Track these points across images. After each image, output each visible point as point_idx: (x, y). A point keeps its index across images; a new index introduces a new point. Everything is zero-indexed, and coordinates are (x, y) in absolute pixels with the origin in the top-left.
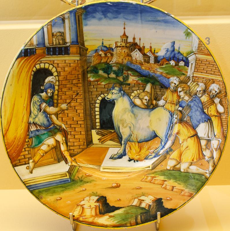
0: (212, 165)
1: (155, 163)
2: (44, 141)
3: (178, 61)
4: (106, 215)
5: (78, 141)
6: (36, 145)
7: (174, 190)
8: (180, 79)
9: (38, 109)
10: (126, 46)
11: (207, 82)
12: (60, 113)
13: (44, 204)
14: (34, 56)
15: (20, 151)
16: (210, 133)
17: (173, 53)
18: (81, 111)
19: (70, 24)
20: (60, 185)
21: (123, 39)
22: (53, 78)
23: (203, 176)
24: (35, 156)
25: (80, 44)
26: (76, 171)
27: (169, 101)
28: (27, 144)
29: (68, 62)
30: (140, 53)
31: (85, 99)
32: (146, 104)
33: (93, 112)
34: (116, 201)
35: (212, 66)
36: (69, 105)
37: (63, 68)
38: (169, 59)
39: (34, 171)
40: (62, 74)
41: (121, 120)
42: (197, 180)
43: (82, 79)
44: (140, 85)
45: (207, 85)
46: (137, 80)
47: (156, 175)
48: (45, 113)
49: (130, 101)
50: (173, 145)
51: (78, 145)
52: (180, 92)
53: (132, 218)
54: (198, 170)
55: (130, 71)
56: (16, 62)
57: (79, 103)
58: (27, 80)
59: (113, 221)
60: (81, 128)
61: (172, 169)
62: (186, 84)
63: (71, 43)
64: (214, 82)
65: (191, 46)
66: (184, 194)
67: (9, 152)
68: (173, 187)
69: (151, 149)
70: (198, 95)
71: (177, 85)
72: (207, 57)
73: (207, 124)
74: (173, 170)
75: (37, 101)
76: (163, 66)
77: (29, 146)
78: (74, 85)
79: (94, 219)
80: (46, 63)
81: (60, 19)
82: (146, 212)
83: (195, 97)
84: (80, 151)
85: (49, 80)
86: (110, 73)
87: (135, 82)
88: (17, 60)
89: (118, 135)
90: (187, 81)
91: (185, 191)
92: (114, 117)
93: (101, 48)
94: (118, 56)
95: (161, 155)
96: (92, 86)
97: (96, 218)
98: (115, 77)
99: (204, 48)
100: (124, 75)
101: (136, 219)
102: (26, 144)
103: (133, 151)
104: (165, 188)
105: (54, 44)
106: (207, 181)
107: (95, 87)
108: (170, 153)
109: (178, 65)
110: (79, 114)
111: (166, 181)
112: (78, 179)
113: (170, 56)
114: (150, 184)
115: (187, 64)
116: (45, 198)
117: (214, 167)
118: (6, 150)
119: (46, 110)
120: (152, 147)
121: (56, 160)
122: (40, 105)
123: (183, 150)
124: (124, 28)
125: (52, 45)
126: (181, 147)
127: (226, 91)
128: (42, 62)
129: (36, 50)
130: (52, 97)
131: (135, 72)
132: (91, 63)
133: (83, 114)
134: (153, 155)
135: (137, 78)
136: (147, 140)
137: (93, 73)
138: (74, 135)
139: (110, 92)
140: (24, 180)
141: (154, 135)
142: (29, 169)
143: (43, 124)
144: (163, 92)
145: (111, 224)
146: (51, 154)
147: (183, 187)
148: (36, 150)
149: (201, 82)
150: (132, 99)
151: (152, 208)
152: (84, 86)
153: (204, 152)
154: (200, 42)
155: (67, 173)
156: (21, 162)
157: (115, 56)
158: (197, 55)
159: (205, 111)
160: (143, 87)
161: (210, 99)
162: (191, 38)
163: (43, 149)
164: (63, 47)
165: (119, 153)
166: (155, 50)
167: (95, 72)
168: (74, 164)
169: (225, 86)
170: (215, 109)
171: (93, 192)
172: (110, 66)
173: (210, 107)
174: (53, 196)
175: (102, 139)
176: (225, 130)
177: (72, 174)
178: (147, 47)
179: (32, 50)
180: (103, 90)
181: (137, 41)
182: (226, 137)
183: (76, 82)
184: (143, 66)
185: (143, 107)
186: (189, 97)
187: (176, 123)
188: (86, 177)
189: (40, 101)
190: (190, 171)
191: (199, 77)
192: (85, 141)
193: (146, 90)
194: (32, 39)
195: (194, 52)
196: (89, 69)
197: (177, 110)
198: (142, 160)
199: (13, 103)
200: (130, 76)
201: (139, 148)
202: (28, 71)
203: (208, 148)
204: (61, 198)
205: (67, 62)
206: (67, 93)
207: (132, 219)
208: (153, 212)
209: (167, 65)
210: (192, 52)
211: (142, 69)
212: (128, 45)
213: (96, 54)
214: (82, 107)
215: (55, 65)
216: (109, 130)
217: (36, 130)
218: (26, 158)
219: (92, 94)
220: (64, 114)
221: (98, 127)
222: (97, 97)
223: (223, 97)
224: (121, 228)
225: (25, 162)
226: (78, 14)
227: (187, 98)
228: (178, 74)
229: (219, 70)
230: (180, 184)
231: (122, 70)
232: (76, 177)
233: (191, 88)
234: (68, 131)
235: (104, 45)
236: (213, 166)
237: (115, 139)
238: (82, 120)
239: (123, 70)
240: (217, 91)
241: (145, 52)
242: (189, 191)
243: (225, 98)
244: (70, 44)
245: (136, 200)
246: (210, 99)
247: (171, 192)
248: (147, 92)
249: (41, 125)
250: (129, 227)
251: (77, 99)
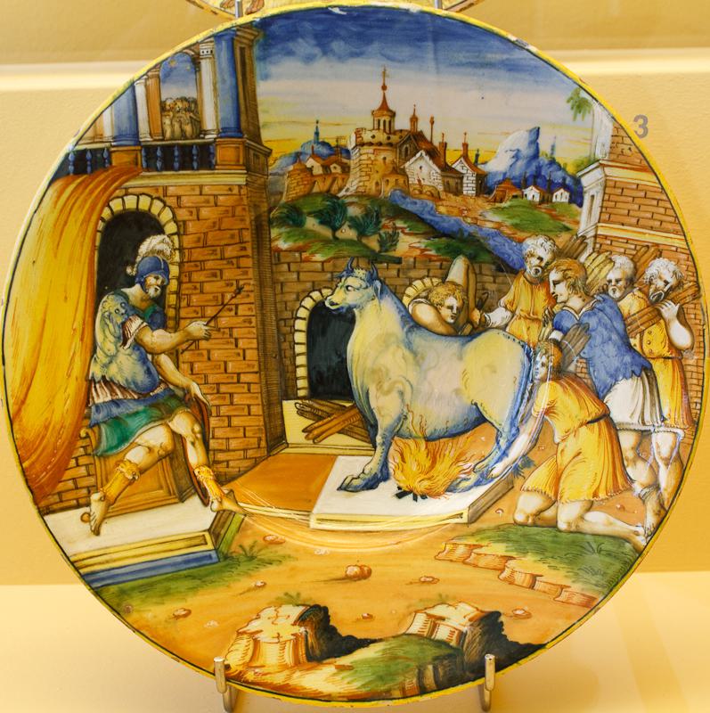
0: (655, 508)
1: (478, 504)
2: (137, 435)
3: (549, 188)
4: (327, 664)
5: (241, 434)
6: (111, 448)
7: (538, 585)
8: (557, 243)
9: (119, 338)
10: (390, 141)
11: (639, 254)
12: (186, 349)
13: (136, 630)
14: (106, 174)
15: (62, 467)
16: (649, 411)
17: (534, 164)
18: (249, 343)
19: (218, 75)
20: (185, 572)
21: (379, 121)
22: (163, 241)
23: (627, 544)
24: (107, 481)
25: (246, 136)
26: (234, 527)
27: (522, 310)
28: (84, 445)
29: (210, 192)
30: (431, 162)
31: (262, 306)
32: (452, 321)
33: (288, 347)
34: (358, 620)
35: (655, 203)
36: (212, 324)
37: (194, 211)
38: (522, 184)
39: (104, 529)
40: (191, 227)
41: (374, 372)
42: (609, 554)
43: (252, 244)
44: (432, 263)
45: (638, 264)
46: (423, 246)
47: (482, 539)
48: (139, 349)
49: (400, 311)
51: (242, 448)
52: (556, 283)
53: (407, 672)
54: (611, 524)
55: (402, 219)
56: (50, 192)
57: (243, 318)
58: (82, 246)
59: (349, 683)
60: (249, 395)
61: (530, 521)
62: (576, 259)
63: (219, 133)
64: (661, 253)
65: (591, 142)
66: (569, 598)
67: (27, 468)
68: (534, 577)
69: (466, 461)
70: (611, 293)
71: (547, 264)
72: (639, 177)
73: (640, 382)
74: (534, 525)
75: (113, 311)
76: (504, 205)
77: (89, 451)
78: (228, 263)
79: (289, 677)
80: (141, 195)
81: (186, 57)
82: (450, 656)
83: (601, 299)
84: (246, 465)
85: (151, 246)
86: (341, 226)
87: (417, 253)
88: (53, 185)
89: (364, 416)
90: (577, 250)
92: (352, 360)
93: (313, 147)
95: (496, 480)
96: (286, 266)
97: (298, 674)
98: (356, 239)
99: (630, 149)
100: (382, 232)
101: (421, 676)
102: (80, 443)
103: (412, 467)
104: (510, 581)
105: (168, 134)
106: (640, 559)
107: (293, 267)
108: (526, 471)
109: (549, 201)
110: (244, 350)
111: (511, 558)
112: (242, 552)
113: (526, 173)
114: (464, 566)
115: (577, 196)
116: (139, 611)
117: (661, 516)
118: (18, 464)
119: (141, 340)
120: (468, 455)
121: (174, 494)
122: (123, 324)
123: (565, 463)
124: (384, 88)
125: (161, 138)
126: (559, 454)
127: (697, 282)
128: (130, 190)
129: (110, 153)
130: (160, 300)
131: (417, 221)
132: (281, 193)
133: (256, 352)
134: (474, 477)
135: (423, 240)
136: (454, 432)
137: (288, 225)
138: (229, 417)
139: (340, 284)
140: (75, 555)
141: (474, 416)
142: (90, 521)
143: (134, 383)
144: (503, 283)
145: (342, 691)
146: (158, 476)
147: (566, 576)
148: (112, 462)
149: (620, 254)
150: (406, 304)
151: (468, 644)
152: (259, 264)
153: (629, 470)
154: (617, 129)
155: (207, 534)
156: (64, 499)
157: (354, 171)
158: (607, 170)
159: (632, 341)
160: (441, 268)
161: (648, 307)
162: (591, 118)
163: (133, 460)
164: (195, 144)
165: (366, 471)
166: (477, 156)
167: (294, 221)
168: (228, 505)
169: (695, 266)
170: (663, 335)
171: (286, 594)
172: (339, 205)
173: (649, 329)
174: (163, 604)
175: (316, 428)
176: (695, 400)
177: (222, 536)
178: (454, 146)
179: (99, 155)
180: (319, 279)
181: (423, 126)
182: (698, 424)
183: (235, 254)
184: (440, 203)
185: (441, 329)
186: (584, 300)
187: (543, 380)
188: (266, 547)
189: (123, 311)
190: (585, 527)
191: (615, 237)
192: (264, 435)
193: (450, 277)
194: (98, 121)
195: (598, 161)
196: (275, 213)
197: (547, 339)
198: (437, 495)
199: (39, 317)
200: (401, 235)
201: (429, 457)
202: (87, 220)
203: (643, 456)
204: (189, 612)
205: (206, 190)
206: (207, 287)
207: (407, 675)
208: (471, 654)
209: (515, 202)
210: (591, 161)
211: (440, 213)
212: (395, 139)
213: (297, 166)
214: (254, 330)
215: (171, 201)
216: (337, 402)
217: (112, 401)
218: (81, 488)
219: (285, 289)
220: (197, 352)
221: (302, 393)
222: (301, 299)
223: (688, 299)
224: (373, 703)
225: (78, 501)
226: (241, 42)
227: (576, 302)
228: (551, 227)
229: (677, 217)
230: (555, 568)
231: (377, 215)
232: (234, 547)
233: (589, 271)
234: (211, 403)
235: (320, 140)
236: (658, 514)
237: (356, 429)
238: (252, 370)
239: (378, 216)
240: (669, 280)
241: (449, 160)
242: (583, 589)
243: (695, 301)
244: (215, 136)
245: (421, 618)
246: (648, 307)
247: (529, 593)
248: (453, 283)
249: (126, 386)
250: (397, 701)
251: (237, 306)
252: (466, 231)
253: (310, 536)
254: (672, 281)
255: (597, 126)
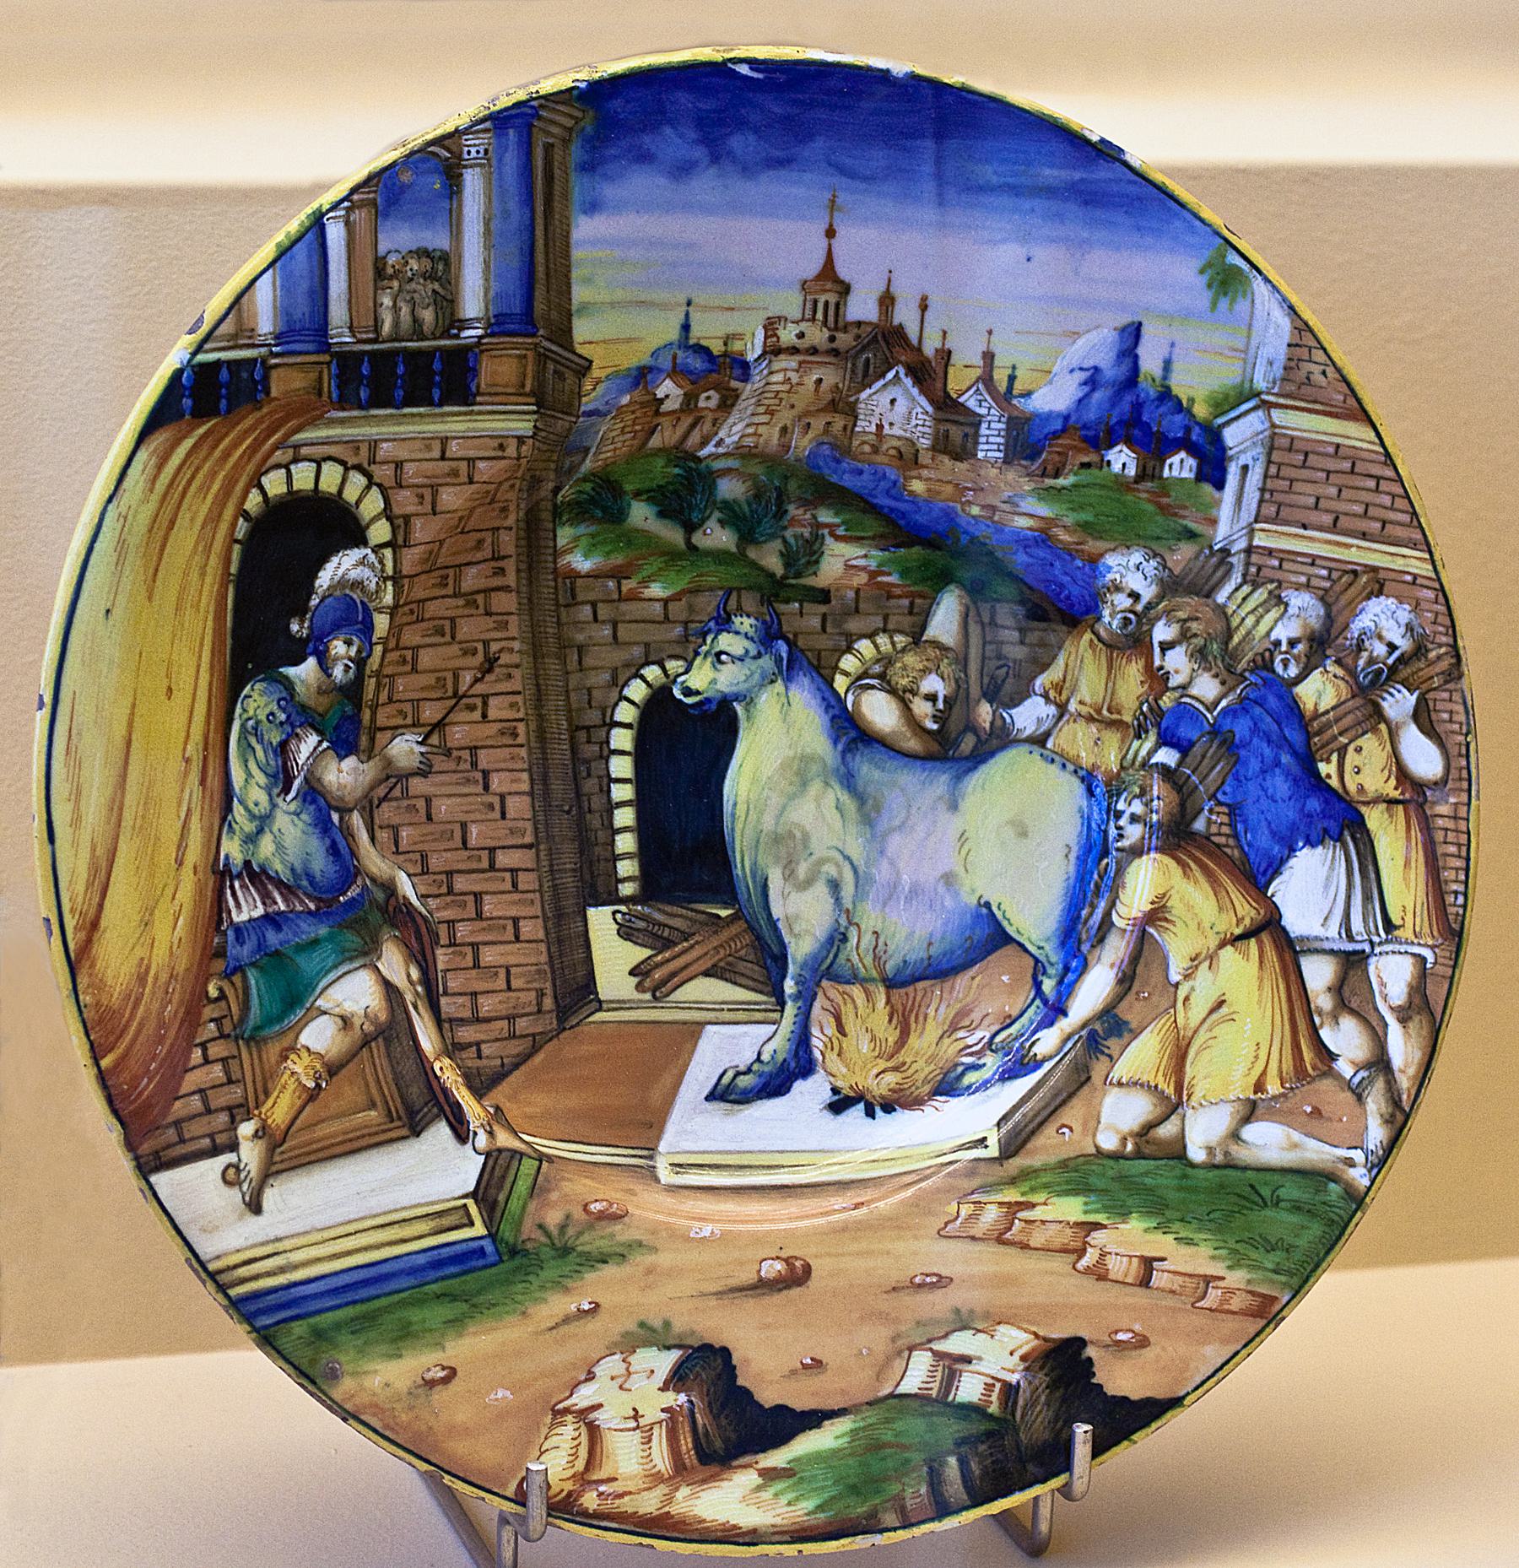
0: (1384, 1110)
1: (1017, 1116)
2: (318, 990)
3: (1154, 448)
4: (741, 1467)
5: (501, 983)
6: (270, 1021)
7: (1158, 1279)
8: (1169, 564)
9: (274, 776)
10: (834, 345)
11: (1337, 588)
12: (385, 798)
13: (347, 1415)
14: (258, 414)
15: (177, 1067)
16: (1360, 909)
17: (1129, 397)
18: (512, 783)
19: (494, 204)
20: (434, 1287)
21: (815, 302)
22: (362, 562)
23: (1332, 1186)
24: (267, 1094)
25: (541, 332)
26: (522, 1186)
27: (1081, 702)
28: (215, 1015)
29: (459, 454)
30: (915, 391)
31: (539, 699)
32: (935, 727)
33: (597, 789)
34: (793, 1372)
35: (1372, 484)
36: (434, 740)
37: (427, 493)
38: (1099, 439)
39: (270, 1198)
40: (422, 531)
41: (777, 839)
42: (1297, 1208)
43: (518, 561)
44: (893, 602)
45: (1335, 609)
46: (873, 564)
47: (1033, 1190)
48: (314, 801)
49: (828, 707)
51: (504, 1013)
52: (1166, 647)
53: (906, 1474)
54: (1295, 1146)
55: (829, 506)
56: (142, 455)
57: (499, 726)
58: (203, 574)
59: (789, 1504)
60: (516, 896)
61: (1130, 1147)
62: (1208, 596)
63: (489, 325)
64: (1382, 586)
65: (1246, 355)
66: (1224, 1301)
67: (107, 1070)
68: (1148, 1263)
69: (971, 1029)
70: (1279, 668)
71: (1149, 606)
72: (1341, 432)
73: (1340, 854)
74: (1139, 1155)
75: (263, 717)
76: (1061, 482)
77: (227, 1029)
78: (468, 604)
79: (669, 1499)
80: (325, 460)
81: (433, 163)
82: (989, 1434)
83: (1260, 681)
84: (515, 1051)
85: (340, 572)
86: (703, 521)
87: (863, 578)
88: (147, 441)
89: (759, 938)
90: (1208, 580)
92: (733, 815)
93: (675, 357)
94: (762, 409)
95: (1048, 1066)
96: (588, 609)
97: (684, 1491)
98: (734, 549)
99: (1324, 373)
100: (788, 534)
101: (935, 1479)
102: (209, 1012)
103: (860, 1045)
104: (1099, 1273)
105: (387, 328)
106: (1359, 1214)
107: (604, 611)
108: (1113, 1044)
109: (1155, 475)
110: (502, 797)
111: (1098, 1226)
112: (544, 1239)
113: (1109, 417)
114: (1002, 1248)
115: (1213, 468)
116: (355, 1374)
117: (1398, 1125)
118: (89, 1062)
119: (319, 780)
120: (976, 1016)
121: (400, 1118)
122: (284, 745)
123: (1193, 1023)
124: (830, 233)
125: (371, 336)
126: (1180, 1004)
127: (1455, 646)
128: (304, 451)
129: (268, 369)
130: (352, 692)
131: (864, 512)
132: (587, 450)
133: (527, 799)
134: (992, 1062)
135: (874, 553)
136: (945, 966)
137: (593, 519)
138: (475, 946)
139: (705, 648)
140: (218, 1257)
141: (981, 933)
142: (240, 1184)
143: (307, 875)
144: (1042, 644)
145: (778, 1520)
146: (365, 1079)
147: (1213, 1258)
148: (273, 1050)
149: (1298, 587)
150: (842, 691)
151: (1025, 1407)
152: (530, 605)
153: (1325, 1034)
154: (1300, 331)
155: (470, 1203)
156: (187, 1136)
157: (746, 405)
158: (1277, 415)
159: (1323, 768)
160: (911, 613)
161: (1353, 697)
162: (1248, 303)
163: (317, 1046)
164: (438, 348)
165: (765, 1057)
166: (1012, 379)
167: (604, 510)
168: (504, 1139)
169: (1450, 615)
170: (1384, 755)
171: (642, 1325)
172: (699, 474)
173: (1359, 742)
174: (400, 1356)
175: (662, 964)
176: (1454, 887)
177: (502, 1204)
178: (967, 356)
179: (245, 375)
180: (657, 638)
181: (905, 315)
182: (1460, 934)
183: (483, 583)
184: (914, 473)
185: (913, 744)
186: (1223, 683)
187: (1137, 851)
188: (591, 1227)
189: (283, 717)
190: (1242, 1154)
191: (1289, 552)
192: (548, 985)
193: (931, 632)
194: (245, 299)
195: (1258, 394)
196: (566, 493)
197: (1144, 765)
198: (914, 1103)
199: (120, 730)
200: (829, 540)
201: (895, 1021)
202: (214, 518)
203: (1354, 1005)
204: (452, 1373)
205: (454, 448)
206: (426, 659)
207: (906, 1480)
208: (1036, 1425)
209: (1085, 476)
210: (1241, 397)
211: (911, 493)
212: (845, 340)
213: (638, 395)
214: (523, 752)
215: (383, 473)
216: (702, 907)
217: (266, 917)
218: (216, 1111)
219: (589, 661)
220: (405, 803)
221: (627, 889)
222: (620, 683)
223: (1436, 682)
224: (843, 1541)
225: (213, 1140)
226: (548, 133)
227: (1207, 687)
228: (1158, 532)
229: (1414, 514)
230: (1190, 1242)
231: (779, 496)
232: (528, 1229)
233: (1235, 622)
234: (438, 915)
235: (692, 342)
236: (1388, 1121)
237: (742, 967)
238: (520, 842)
239: (781, 497)
240: (1398, 641)
241: (953, 386)
242: (1249, 1282)
243: (1450, 686)
244: (480, 332)
245: (921, 1362)
246: (1353, 697)
247: (1140, 1297)
248: (936, 644)
249: (291, 882)
250: (891, 1534)
251: (485, 698)
252: (966, 532)
255: (1258, 324)
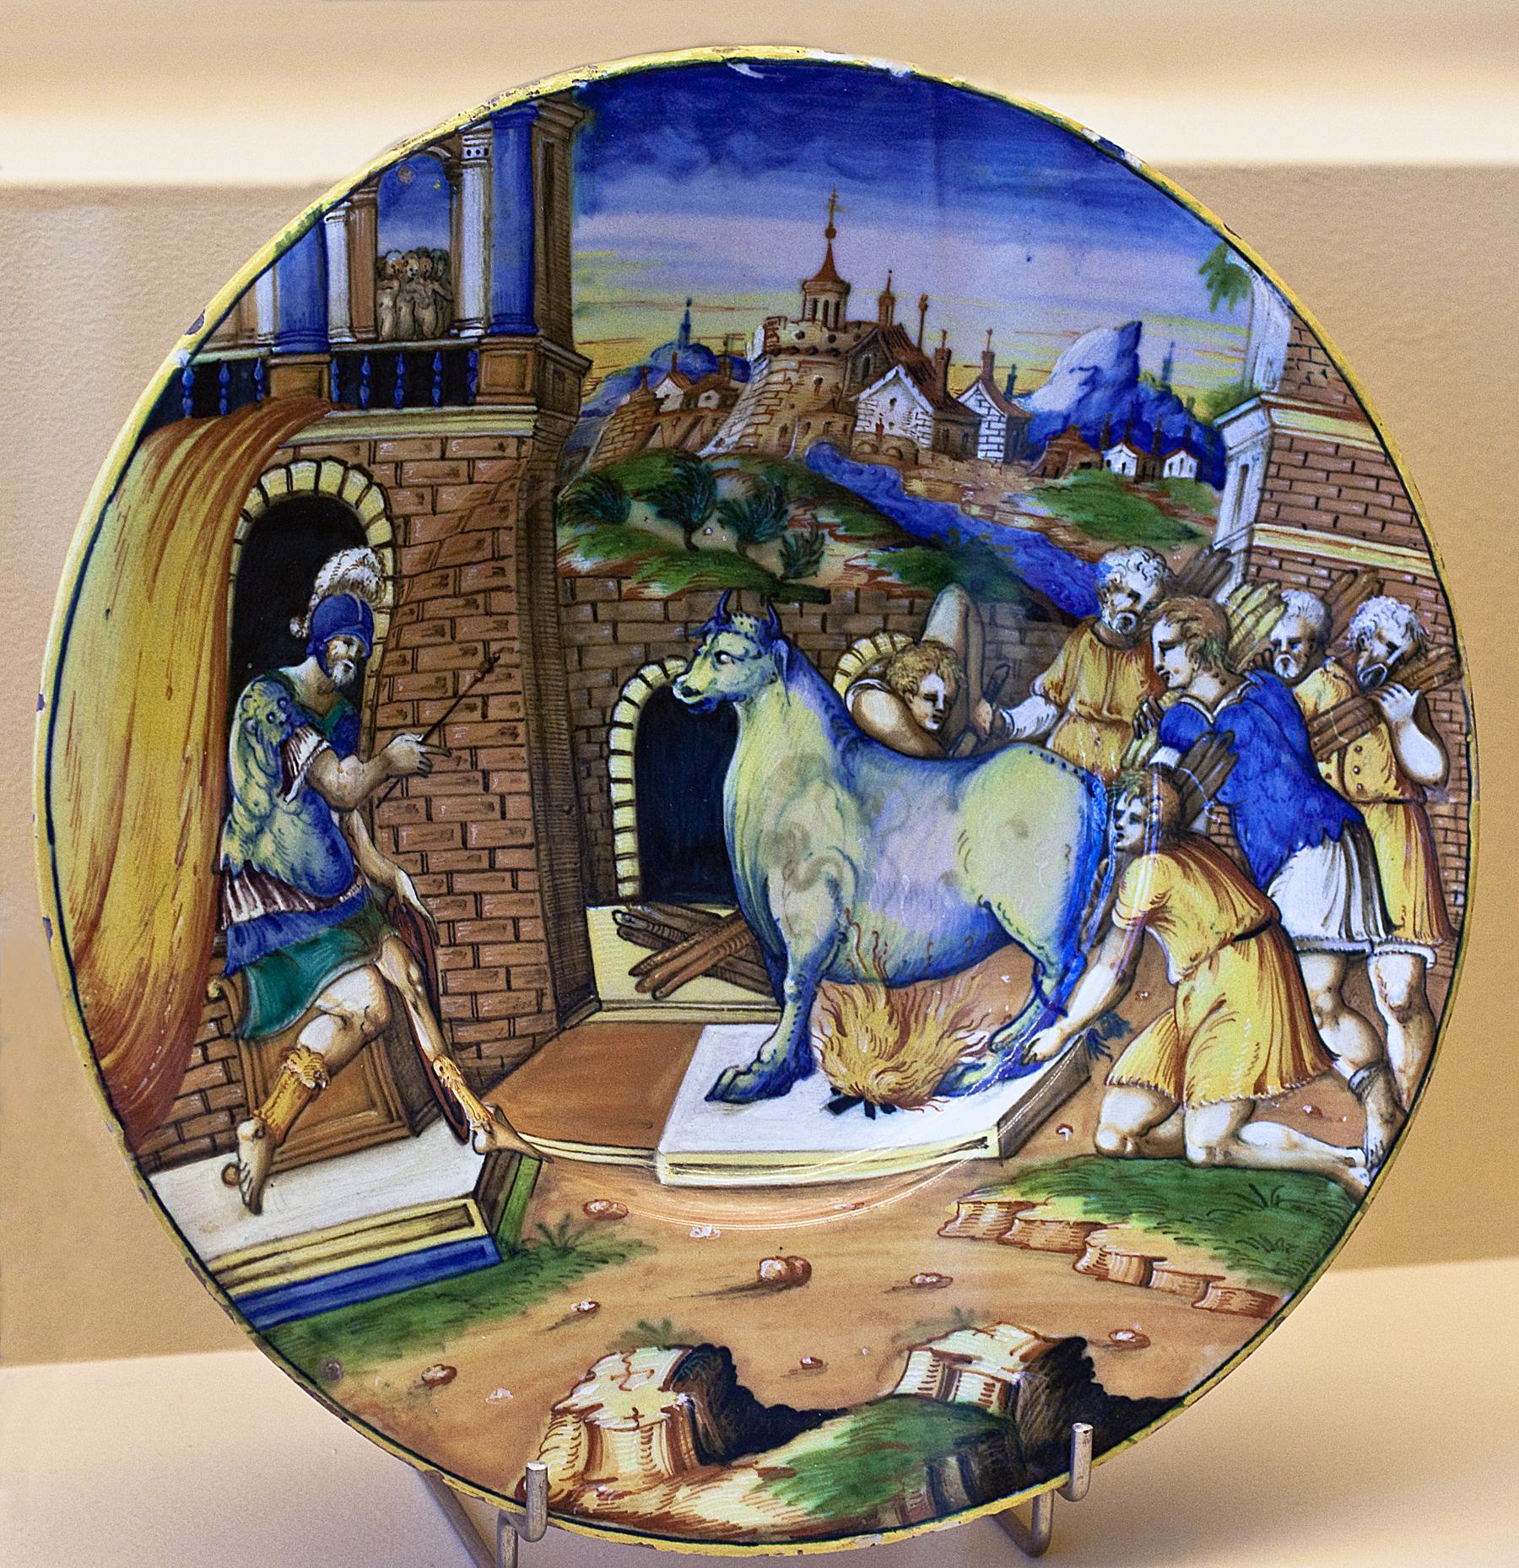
0: (1384, 1110)
1: (1017, 1116)
2: (318, 990)
3: (1154, 448)
4: (741, 1467)
5: (501, 983)
6: (270, 1021)
7: (1158, 1279)
8: (1169, 564)
9: (274, 776)
10: (834, 345)
11: (1337, 588)
12: (385, 798)
13: (347, 1415)
14: (258, 414)
15: (177, 1067)
16: (1360, 909)
17: (1129, 397)
18: (512, 783)
19: (494, 204)
20: (434, 1287)
21: (815, 302)
22: (362, 562)
23: (1332, 1186)
24: (267, 1094)
25: (541, 332)
26: (522, 1186)
27: (1081, 702)
28: (215, 1015)
29: (459, 454)
30: (915, 391)
31: (539, 699)
32: (935, 727)
33: (597, 789)
34: (793, 1372)
35: (1372, 484)
36: (434, 740)
37: (427, 493)
38: (1099, 439)
39: (270, 1198)
40: (422, 531)
41: (777, 839)
42: (1297, 1208)
43: (518, 561)
44: (893, 602)
45: (1335, 609)
46: (873, 564)
47: (1033, 1190)
48: (314, 801)
49: (828, 707)
50: (1131, 996)
51: (504, 1013)
52: (1166, 647)
53: (906, 1474)
54: (1295, 1146)
55: (829, 506)
56: (142, 455)
57: (499, 726)
58: (203, 574)
59: (789, 1504)
60: (516, 896)
61: (1130, 1147)
62: (1208, 596)
63: (489, 325)
64: (1382, 586)
65: (1246, 355)
66: (1224, 1301)
67: (107, 1070)
68: (1148, 1263)
69: (971, 1029)
70: (1279, 668)
71: (1149, 606)
72: (1341, 432)
73: (1340, 854)
74: (1139, 1155)
75: (263, 717)
76: (1061, 482)
77: (227, 1029)
78: (468, 604)
79: (669, 1499)
80: (325, 460)
81: (433, 163)
82: (989, 1434)
83: (1260, 681)
84: (515, 1051)
85: (340, 572)
86: (703, 521)
87: (863, 578)
88: (147, 441)
89: (759, 938)
90: (1208, 580)
91: (1221, 1284)
92: (733, 815)
93: (675, 357)
94: (762, 409)
95: (1048, 1066)
96: (588, 609)
97: (684, 1491)
98: (734, 549)
99: (1324, 373)
100: (788, 534)
101: (935, 1479)
102: (209, 1012)
103: (860, 1045)
104: (1099, 1273)
105: (387, 328)
106: (1359, 1214)
107: (604, 611)
108: (1113, 1044)
109: (1155, 475)
110: (502, 797)
111: (1098, 1226)
112: (544, 1239)
113: (1109, 417)
114: (1002, 1248)
115: (1213, 468)
116: (355, 1374)
117: (1398, 1125)
118: (89, 1062)
119: (319, 780)
120: (976, 1016)
121: (400, 1118)
122: (284, 745)
123: (1193, 1023)
124: (830, 233)
125: (371, 336)
126: (1180, 1004)
127: (1455, 646)
128: (304, 451)
129: (268, 369)
130: (352, 692)
131: (864, 512)
132: (587, 450)
133: (527, 799)
134: (992, 1062)
135: (874, 553)
136: (945, 966)
137: (593, 519)
138: (475, 946)
139: (705, 648)
140: (218, 1257)
141: (981, 933)
142: (240, 1184)
143: (307, 875)
144: (1042, 644)
145: (778, 1520)
146: (365, 1079)
147: (1213, 1258)
148: (273, 1050)
149: (1298, 587)
150: (842, 691)
151: (1025, 1407)
152: (530, 605)
153: (1325, 1034)
154: (1300, 331)
155: (470, 1203)
156: (187, 1136)
157: (746, 405)
158: (1277, 415)
159: (1323, 768)
160: (911, 613)
161: (1353, 697)
162: (1248, 303)
163: (317, 1046)
164: (438, 348)
165: (765, 1057)
166: (1012, 379)
167: (604, 510)
168: (504, 1139)
169: (1450, 615)
170: (1384, 755)
171: (642, 1325)
172: (699, 474)
173: (1359, 742)
174: (400, 1356)
175: (662, 964)
176: (1454, 887)
177: (502, 1204)
178: (967, 356)
179: (245, 375)
180: (657, 638)
181: (905, 315)
182: (1460, 934)
183: (483, 583)
184: (914, 473)
185: (913, 744)
186: (1223, 683)
187: (1137, 851)
188: (591, 1227)
189: (283, 717)
190: (1242, 1154)
191: (1289, 552)
192: (548, 985)
193: (931, 632)
194: (245, 299)
195: (1258, 394)
196: (566, 493)
197: (1144, 765)
198: (914, 1103)
199: (120, 730)
200: (829, 540)
201: (895, 1021)
202: (214, 518)
203: (1354, 1005)
204: (452, 1373)
205: (454, 448)
206: (426, 659)
207: (906, 1480)
208: (1036, 1425)
209: (1085, 476)
210: (1241, 397)
211: (911, 493)
212: (845, 340)
213: (638, 395)
214: (523, 752)
216: (702, 907)
217: (266, 917)
218: (216, 1111)
219: (589, 661)
220: (405, 803)
221: (627, 889)
222: (620, 683)
223: (1436, 682)
224: (843, 1541)
225: (213, 1140)
226: (548, 133)
227: (1207, 687)
228: (1158, 532)
229: (1414, 514)
230: (1190, 1242)
231: (779, 496)
232: (528, 1229)
233: (1235, 622)
234: (438, 915)
235: (692, 342)
236: (1388, 1121)
237: (742, 967)
238: (520, 842)
239: (781, 497)
240: (1398, 641)
241: (953, 386)
242: (1249, 1282)
243: (1450, 686)
244: (480, 332)
245: (921, 1362)
246: (1353, 697)
247: (1140, 1297)
248: (936, 644)
249: (291, 882)
250: (891, 1534)
251: (485, 698)
252: (966, 532)
253: (669, 1201)
254: (1404, 644)
